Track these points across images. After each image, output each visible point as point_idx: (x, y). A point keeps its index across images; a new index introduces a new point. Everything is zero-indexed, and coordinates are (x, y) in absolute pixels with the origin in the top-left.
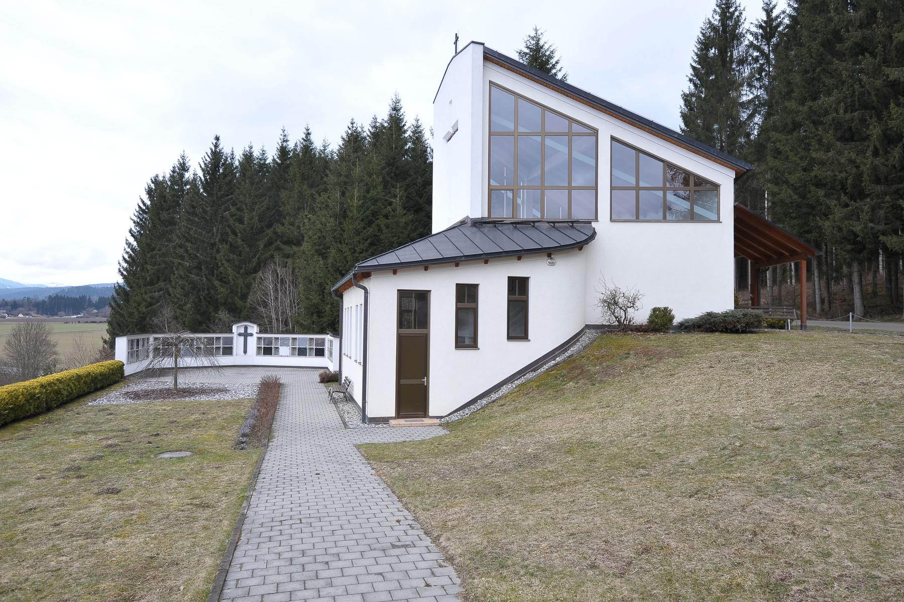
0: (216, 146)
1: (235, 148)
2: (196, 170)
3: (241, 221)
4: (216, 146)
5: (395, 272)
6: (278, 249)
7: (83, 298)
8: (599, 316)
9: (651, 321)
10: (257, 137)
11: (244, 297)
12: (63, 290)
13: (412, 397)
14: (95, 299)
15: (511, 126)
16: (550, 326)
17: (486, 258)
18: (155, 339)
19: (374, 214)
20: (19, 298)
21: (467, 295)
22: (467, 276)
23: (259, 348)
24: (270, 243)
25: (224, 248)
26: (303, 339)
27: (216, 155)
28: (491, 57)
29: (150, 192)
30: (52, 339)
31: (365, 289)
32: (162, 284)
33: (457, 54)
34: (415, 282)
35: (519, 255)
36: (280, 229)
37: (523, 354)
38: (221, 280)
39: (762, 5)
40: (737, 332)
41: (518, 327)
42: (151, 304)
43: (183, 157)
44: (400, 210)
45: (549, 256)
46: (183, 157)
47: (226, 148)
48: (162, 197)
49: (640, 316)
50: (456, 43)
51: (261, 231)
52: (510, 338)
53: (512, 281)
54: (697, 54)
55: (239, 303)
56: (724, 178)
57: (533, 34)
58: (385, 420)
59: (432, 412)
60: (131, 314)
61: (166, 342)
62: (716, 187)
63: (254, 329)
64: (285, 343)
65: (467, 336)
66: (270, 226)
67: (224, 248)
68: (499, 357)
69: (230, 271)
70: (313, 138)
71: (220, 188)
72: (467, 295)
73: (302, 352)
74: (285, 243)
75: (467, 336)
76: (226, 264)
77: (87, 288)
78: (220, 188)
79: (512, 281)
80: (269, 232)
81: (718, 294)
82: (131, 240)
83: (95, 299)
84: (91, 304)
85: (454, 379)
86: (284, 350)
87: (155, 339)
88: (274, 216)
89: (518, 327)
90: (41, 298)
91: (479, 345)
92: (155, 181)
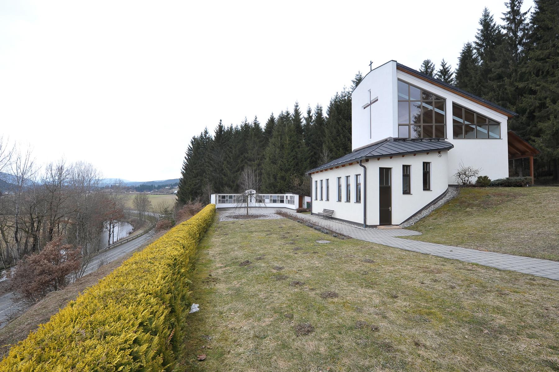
0: (220, 124)
1: (226, 126)
2: (212, 134)
3: (231, 152)
4: (220, 124)
5: (403, 156)
6: (246, 163)
7: (152, 185)
8: (456, 181)
9: (478, 182)
10: (234, 121)
11: (233, 182)
12: (145, 183)
13: (385, 217)
14: (156, 186)
15: (407, 98)
16: (439, 185)
17: (414, 153)
18: (219, 196)
19: (294, 147)
20: (130, 186)
21: (406, 169)
22: (385, 164)
23: (256, 200)
24: (242, 161)
25: (225, 162)
26: (275, 196)
27: (221, 127)
28: (400, 68)
29: (192, 143)
30: (149, 200)
31: (364, 167)
32: (199, 177)
33: (371, 70)
34: (385, 164)
35: (428, 152)
36: (246, 155)
37: (430, 197)
38: (224, 175)
39: (441, 64)
40: (521, 186)
41: (426, 186)
42: (195, 185)
43: (206, 128)
44: (304, 146)
45: (439, 153)
46: (206, 128)
47: (223, 124)
48: (198, 143)
49: (473, 180)
50: (371, 65)
51: (239, 156)
52: (424, 190)
53: (381, 169)
54: (231, 128)
55: (232, 184)
56: (503, 120)
57: (358, 73)
58: (375, 226)
59: (393, 222)
60: (188, 189)
61: (224, 197)
62: (498, 124)
63: (254, 192)
64: (267, 198)
65: (407, 190)
66: (242, 154)
67: (225, 162)
68: (419, 199)
69: (228, 171)
70: (257, 119)
71: (223, 140)
72: (406, 169)
73: (275, 201)
74: (248, 160)
75: (407, 190)
76: (227, 169)
77: (153, 182)
78: (223, 140)
79: (381, 169)
80: (242, 156)
81: (499, 170)
82: (186, 161)
83: (156, 186)
84: (155, 188)
85: (403, 207)
86: (267, 201)
87: (219, 196)
88: (243, 151)
89: (426, 186)
90: (137, 186)
91: (412, 192)
92: (194, 138)
